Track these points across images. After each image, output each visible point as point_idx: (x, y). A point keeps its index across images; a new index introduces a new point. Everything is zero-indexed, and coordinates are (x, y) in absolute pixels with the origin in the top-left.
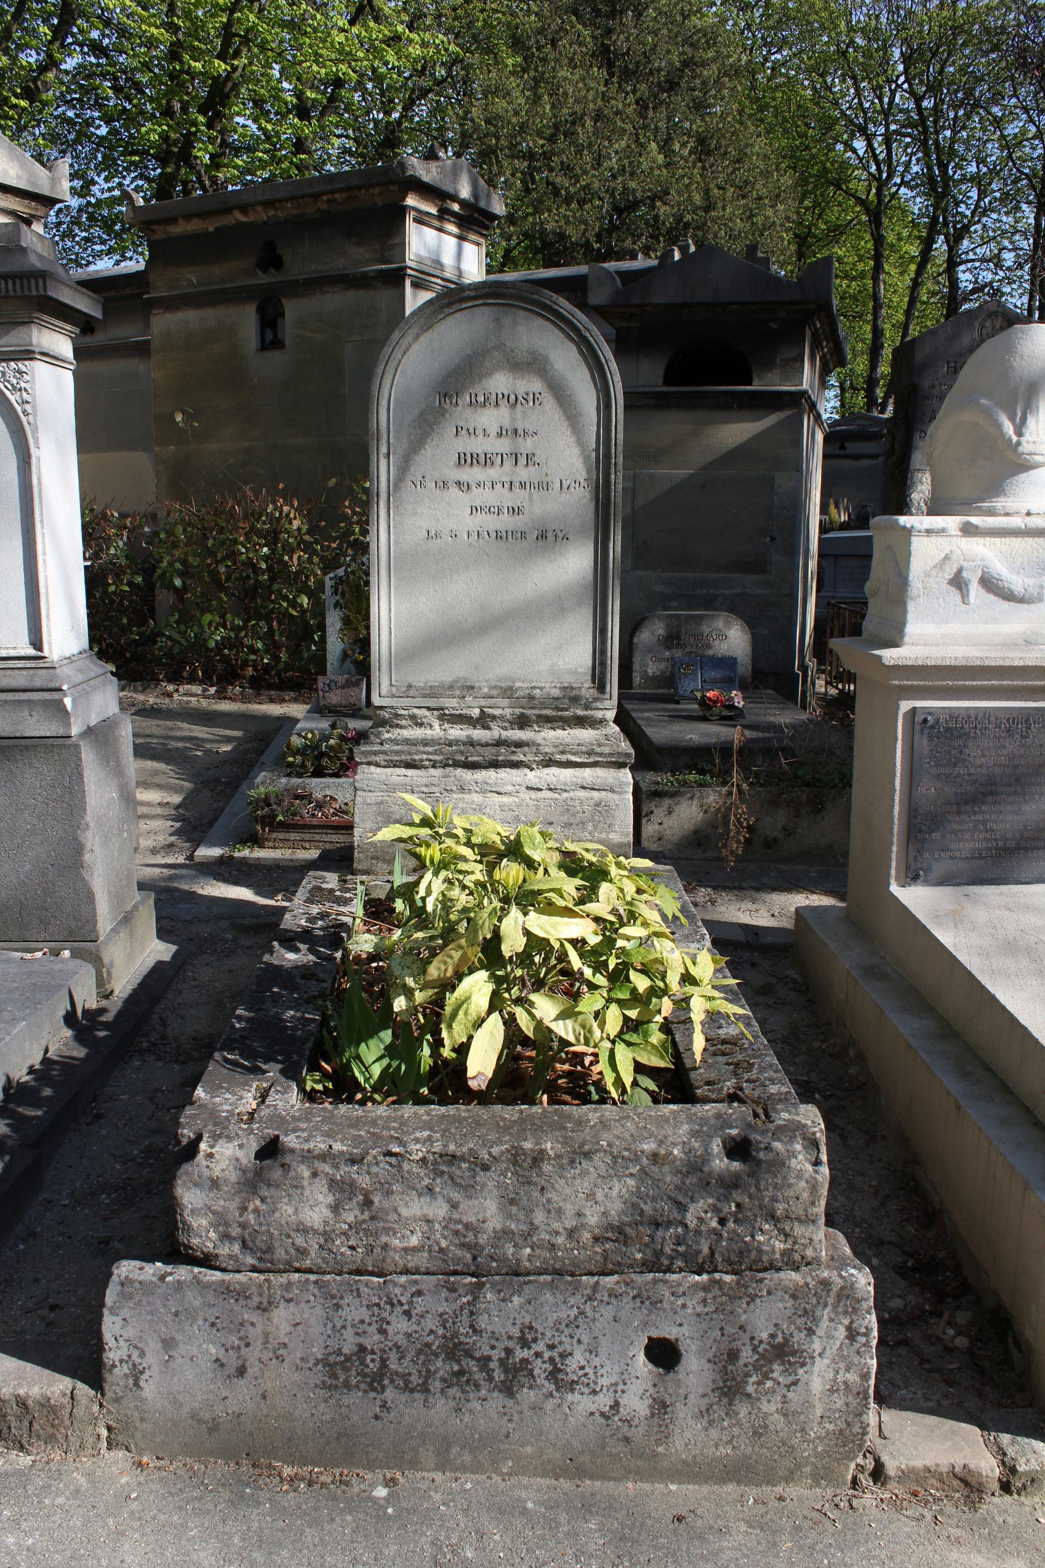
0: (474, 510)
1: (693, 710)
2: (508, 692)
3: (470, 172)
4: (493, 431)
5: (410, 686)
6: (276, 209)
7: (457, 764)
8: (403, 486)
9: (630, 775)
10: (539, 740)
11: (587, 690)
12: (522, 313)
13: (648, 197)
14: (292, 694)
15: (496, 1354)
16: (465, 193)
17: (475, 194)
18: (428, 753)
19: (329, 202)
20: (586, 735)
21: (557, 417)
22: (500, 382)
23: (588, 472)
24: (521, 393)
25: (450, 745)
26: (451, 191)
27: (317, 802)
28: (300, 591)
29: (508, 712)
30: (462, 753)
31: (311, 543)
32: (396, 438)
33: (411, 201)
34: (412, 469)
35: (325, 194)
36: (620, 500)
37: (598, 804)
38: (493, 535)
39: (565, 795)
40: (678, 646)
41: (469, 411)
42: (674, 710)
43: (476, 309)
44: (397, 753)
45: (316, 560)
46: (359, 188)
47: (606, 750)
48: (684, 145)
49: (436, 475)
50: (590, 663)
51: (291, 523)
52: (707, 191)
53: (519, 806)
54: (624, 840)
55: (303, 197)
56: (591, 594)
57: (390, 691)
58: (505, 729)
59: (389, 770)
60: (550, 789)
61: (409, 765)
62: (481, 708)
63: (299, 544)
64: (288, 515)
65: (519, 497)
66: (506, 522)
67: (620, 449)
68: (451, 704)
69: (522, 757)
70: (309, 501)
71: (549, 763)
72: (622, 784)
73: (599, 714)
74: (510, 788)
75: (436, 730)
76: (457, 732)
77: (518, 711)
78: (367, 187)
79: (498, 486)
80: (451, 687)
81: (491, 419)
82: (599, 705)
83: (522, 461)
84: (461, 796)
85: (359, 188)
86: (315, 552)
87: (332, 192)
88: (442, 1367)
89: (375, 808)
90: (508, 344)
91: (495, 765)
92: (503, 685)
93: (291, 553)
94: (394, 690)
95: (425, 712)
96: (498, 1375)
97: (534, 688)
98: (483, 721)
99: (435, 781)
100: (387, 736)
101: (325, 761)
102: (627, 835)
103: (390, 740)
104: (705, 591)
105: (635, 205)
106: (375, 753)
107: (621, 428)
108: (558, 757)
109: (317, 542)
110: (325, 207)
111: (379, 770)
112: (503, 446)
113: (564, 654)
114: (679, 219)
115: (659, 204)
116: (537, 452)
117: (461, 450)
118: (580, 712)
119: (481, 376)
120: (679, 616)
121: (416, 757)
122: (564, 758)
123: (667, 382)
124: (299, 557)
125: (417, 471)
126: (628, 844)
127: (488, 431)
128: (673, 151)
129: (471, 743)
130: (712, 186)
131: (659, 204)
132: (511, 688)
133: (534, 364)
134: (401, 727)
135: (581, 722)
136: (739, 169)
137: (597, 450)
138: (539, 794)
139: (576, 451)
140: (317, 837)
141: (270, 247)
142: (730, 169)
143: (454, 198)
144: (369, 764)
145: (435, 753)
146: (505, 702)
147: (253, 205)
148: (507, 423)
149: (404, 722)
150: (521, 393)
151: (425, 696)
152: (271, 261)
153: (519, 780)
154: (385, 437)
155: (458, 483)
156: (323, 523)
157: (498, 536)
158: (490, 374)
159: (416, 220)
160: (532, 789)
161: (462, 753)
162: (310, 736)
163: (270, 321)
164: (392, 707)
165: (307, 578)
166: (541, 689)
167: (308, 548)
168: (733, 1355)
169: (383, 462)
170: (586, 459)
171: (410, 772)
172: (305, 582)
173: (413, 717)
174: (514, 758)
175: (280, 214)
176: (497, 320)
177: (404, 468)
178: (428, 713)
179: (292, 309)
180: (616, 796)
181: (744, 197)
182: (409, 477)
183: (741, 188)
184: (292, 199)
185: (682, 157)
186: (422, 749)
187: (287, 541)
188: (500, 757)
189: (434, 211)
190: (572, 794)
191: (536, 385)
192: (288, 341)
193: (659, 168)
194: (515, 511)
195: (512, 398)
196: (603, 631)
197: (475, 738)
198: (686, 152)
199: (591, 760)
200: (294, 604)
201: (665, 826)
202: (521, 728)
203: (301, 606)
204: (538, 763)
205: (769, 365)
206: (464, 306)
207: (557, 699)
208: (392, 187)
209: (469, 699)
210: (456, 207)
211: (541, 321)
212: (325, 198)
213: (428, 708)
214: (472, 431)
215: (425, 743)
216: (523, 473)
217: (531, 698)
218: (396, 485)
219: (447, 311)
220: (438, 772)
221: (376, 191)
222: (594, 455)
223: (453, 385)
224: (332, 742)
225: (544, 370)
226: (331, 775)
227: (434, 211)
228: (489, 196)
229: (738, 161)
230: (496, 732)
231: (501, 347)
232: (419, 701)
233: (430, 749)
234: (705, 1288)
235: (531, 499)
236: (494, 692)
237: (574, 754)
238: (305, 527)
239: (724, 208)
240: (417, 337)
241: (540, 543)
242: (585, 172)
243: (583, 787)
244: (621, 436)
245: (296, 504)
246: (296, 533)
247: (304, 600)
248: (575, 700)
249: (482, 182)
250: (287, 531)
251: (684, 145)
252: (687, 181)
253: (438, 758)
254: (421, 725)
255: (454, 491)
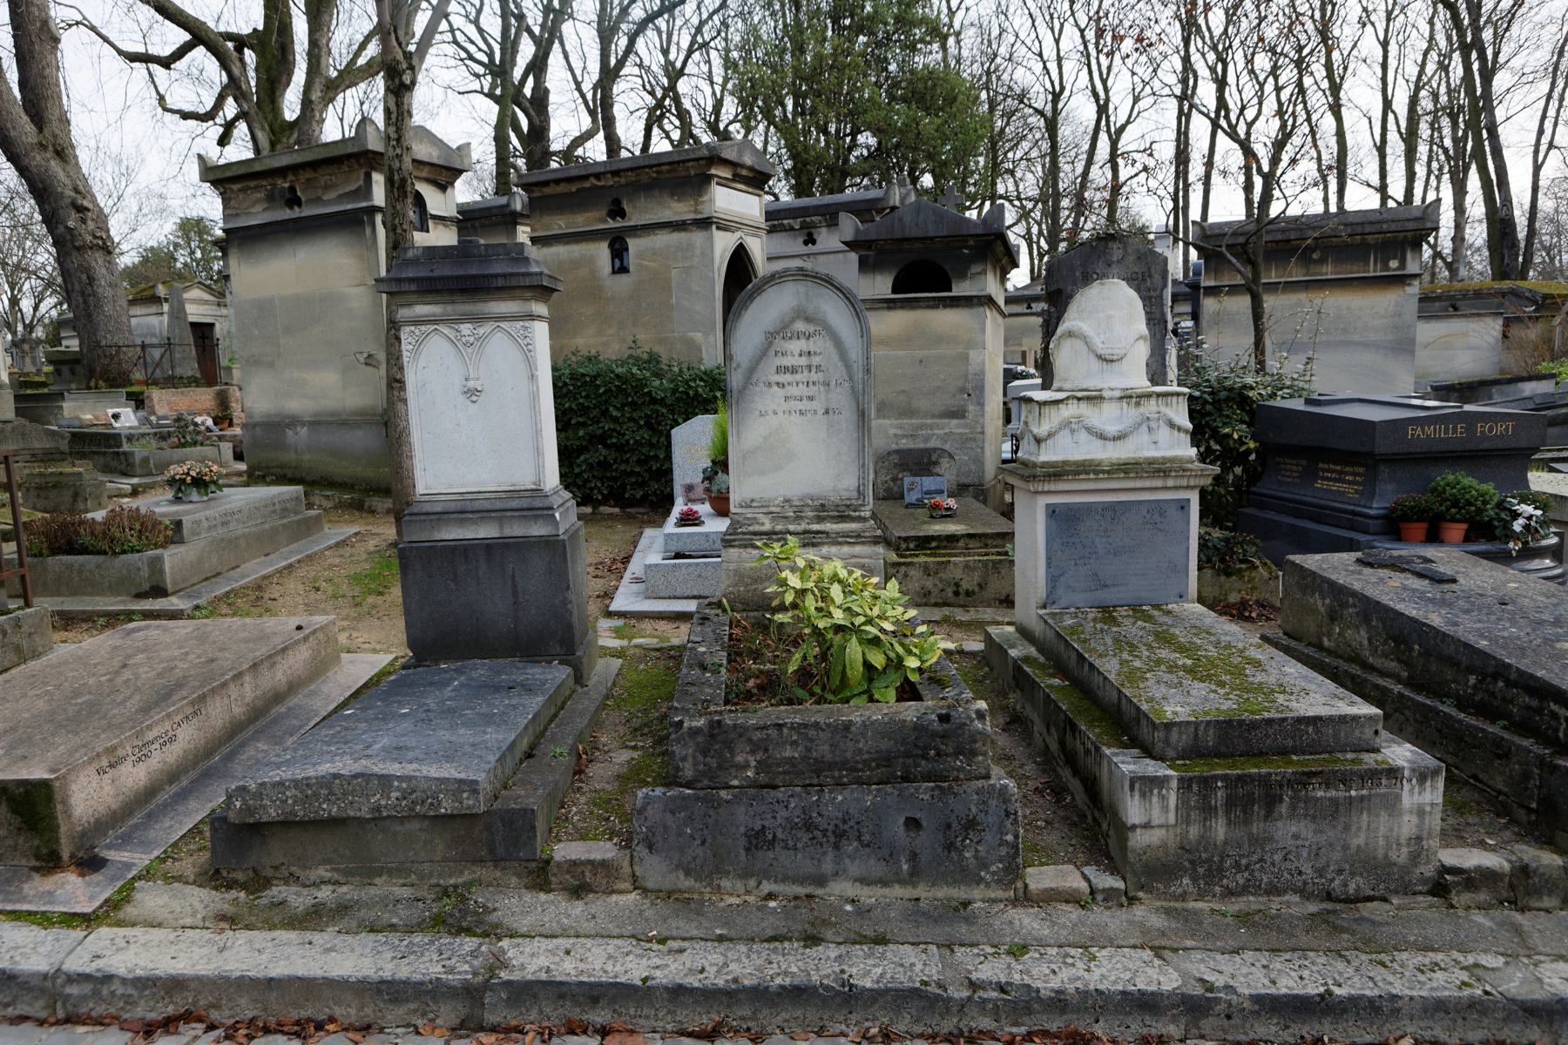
15: (831, 828)
88: (805, 837)
96: (832, 839)
112: (803, 361)
123: (894, 291)
141: (617, 202)
147: (604, 173)
148: (805, 349)
152: (617, 212)
163: (619, 252)
168: (949, 826)
179: (634, 245)
205: (963, 275)
234: (933, 789)
255: (775, 388)
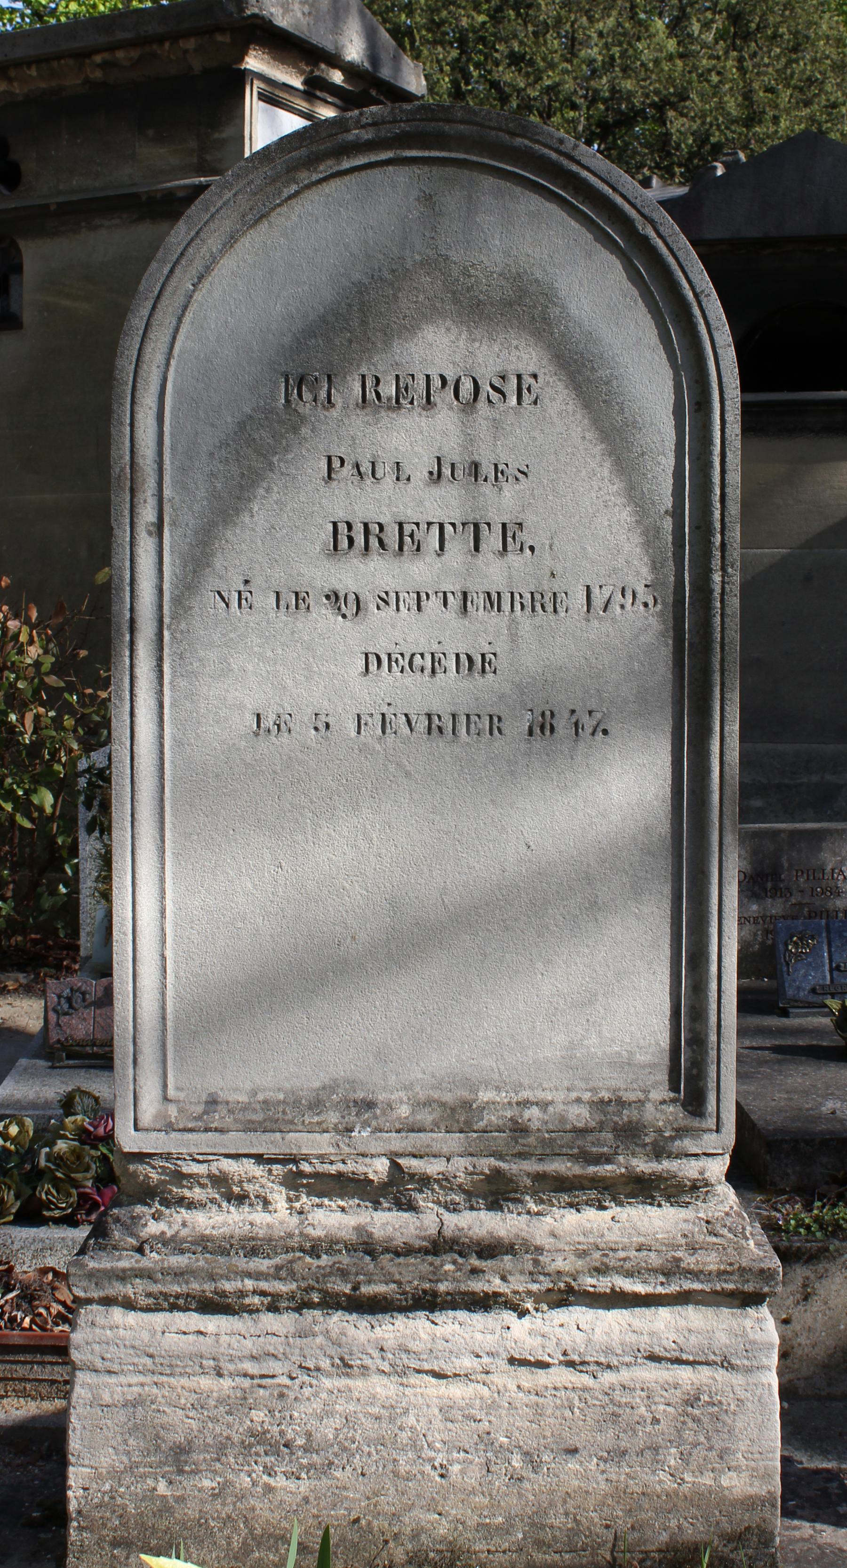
0: (373, 661)
1: (817, 1032)
2: (460, 1115)
3: (362, 15)
4: (419, 467)
5: (212, 1102)
6: (10, 80)
7: (331, 1303)
8: (195, 603)
9: (770, 1324)
10: (540, 1238)
11: (660, 1109)
12: (489, 182)
13: (653, 105)
14: (22, 978)
16: (354, 51)
17: (373, 53)
18: (257, 1276)
19: (104, 65)
20: (658, 1221)
21: (576, 432)
22: (437, 348)
23: (655, 567)
24: (487, 374)
25: (314, 1251)
26: (329, 47)
27: (25, 1287)
28: (37, 781)
29: (460, 1166)
30: (343, 1274)
31: (59, 691)
32: (180, 485)
33: (254, 62)
34: (218, 563)
35: (98, 51)
36: (734, 635)
37: (692, 1401)
38: (421, 725)
39: (608, 1378)
40: (776, 892)
41: (358, 421)
42: (782, 1032)
43: (376, 172)
44: (179, 1274)
45: (68, 722)
46: (160, 40)
47: (711, 1261)
48: (706, 25)
49: (279, 577)
50: (664, 1039)
51: (21, 652)
52: (748, 96)
53: (491, 1407)
54: (759, 1489)
55: (59, 57)
56: (664, 865)
57: (161, 1115)
58: (452, 1208)
59: (159, 1319)
60: (571, 1364)
61: (210, 1306)
62: (393, 1157)
63: (36, 692)
64: (16, 636)
65: (485, 631)
66: (448, 691)
67: (734, 509)
68: (315, 1145)
69: (496, 1284)
70: (60, 609)
71: (565, 1296)
72: (751, 1348)
73: (689, 1169)
74: (467, 1363)
75: (278, 1214)
76: (332, 1218)
77: (486, 1164)
78: (175, 37)
79: (433, 605)
80: (317, 1105)
81: (415, 437)
82: (689, 1144)
83: (492, 540)
84: (342, 1382)
85: (160, 40)
86: (68, 708)
87: (112, 48)
89: (121, 1416)
90: (454, 256)
91: (428, 1302)
92: (448, 1097)
93: (22, 708)
94: (173, 1111)
95: (249, 1167)
97: (525, 1104)
98: (397, 1189)
99: (275, 1345)
100: (153, 1228)
101: (45, 1191)
102: (766, 1476)
103: (163, 1240)
104: (815, 778)
105: (628, 120)
106: (123, 1276)
107: (734, 459)
108: (589, 1282)
109: (71, 688)
110: (98, 74)
111: (132, 1318)
112: (445, 504)
113: (596, 1013)
114: (702, 139)
115: (671, 114)
116: (530, 519)
117: (341, 515)
118: (643, 1166)
119: (388, 336)
120: (776, 833)
121: (228, 1286)
122: (603, 1284)
124: (37, 717)
125: (232, 562)
126: (767, 1501)
127: (407, 470)
128: (690, 36)
129: (367, 1246)
130: (756, 85)
131: (671, 114)
132: (466, 1105)
133: (524, 306)
134: (191, 1205)
135: (644, 1189)
136: (796, 61)
137: (677, 513)
138: (542, 1378)
139: (625, 515)
140: (21, 1371)
142: (783, 60)
143: (334, 60)
144: (108, 1302)
145: (276, 1274)
146: (454, 1141)
149: (197, 1193)
150: (487, 374)
151: (250, 1127)
153: (489, 1341)
154: (151, 483)
155: (333, 597)
156: (83, 653)
157: (434, 726)
158: (410, 329)
159: (262, 97)
160: (524, 1363)
161: (343, 1274)
162: (14, 1130)
164: (168, 1156)
165: (54, 754)
166: (544, 1105)
167: (54, 699)
169: (146, 546)
170: (650, 537)
171: (212, 1323)
172: (49, 765)
173: (220, 1181)
174: (478, 1286)
175: (17, 88)
176: (427, 199)
177: (199, 560)
178: (258, 1171)
180: (737, 1379)
181: (807, 103)
182: (212, 582)
183: (801, 90)
184: (39, 61)
185: (704, 45)
186: (242, 1262)
187: (13, 685)
188: (440, 1281)
189: (297, 82)
190: (625, 1375)
191: (527, 357)
192: (28, 316)
193: (670, 58)
194: (473, 664)
195: (467, 386)
196: (698, 959)
197: (378, 1233)
198: (709, 37)
199: (673, 1288)
200: (25, 806)
201: (796, 1326)
202: (494, 1206)
203: (41, 809)
204: (538, 1298)
206: (346, 165)
207: (583, 1132)
208: (219, 38)
209: (361, 1135)
210: (337, 77)
211: (534, 202)
212: (98, 59)
213: (259, 1159)
214: (366, 467)
215: (252, 1247)
216: (494, 571)
217: (519, 1129)
218: (177, 601)
219: (305, 177)
220: (281, 1323)
221: (190, 44)
222: (668, 524)
223: (321, 358)
224: (61, 1146)
225: (545, 319)
226: (58, 1221)
227: (297, 82)
228: (396, 59)
229: (795, 50)
230: (429, 1218)
231: (436, 263)
232: (236, 1141)
233: (263, 1264)
235: (514, 637)
236: (426, 1117)
237: (629, 1274)
238: (49, 660)
239: (776, 120)
240: (232, 240)
241: (538, 743)
242: (552, 66)
243: (653, 1358)
244: (735, 477)
245: (34, 615)
246: (31, 671)
247: (46, 799)
248: (630, 1133)
249: (385, 36)
250: (13, 668)
251: (706, 25)
252: (715, 78)
253: (282, 1287)
254: (241, 1199)
255: (323, 616)
